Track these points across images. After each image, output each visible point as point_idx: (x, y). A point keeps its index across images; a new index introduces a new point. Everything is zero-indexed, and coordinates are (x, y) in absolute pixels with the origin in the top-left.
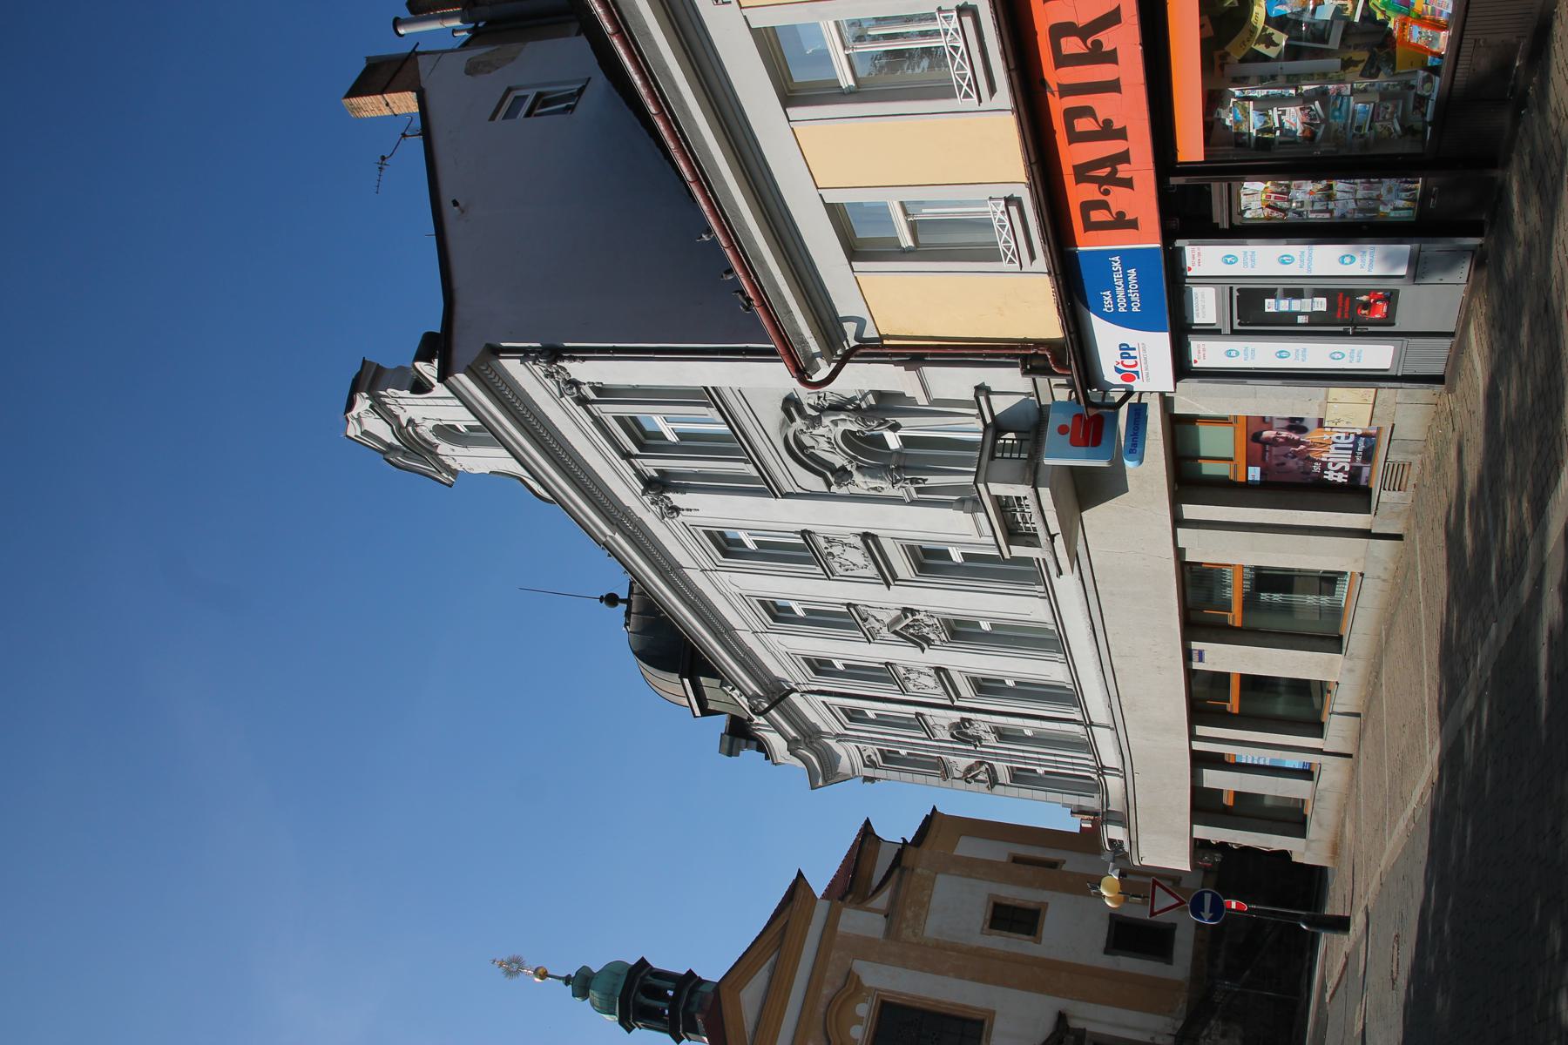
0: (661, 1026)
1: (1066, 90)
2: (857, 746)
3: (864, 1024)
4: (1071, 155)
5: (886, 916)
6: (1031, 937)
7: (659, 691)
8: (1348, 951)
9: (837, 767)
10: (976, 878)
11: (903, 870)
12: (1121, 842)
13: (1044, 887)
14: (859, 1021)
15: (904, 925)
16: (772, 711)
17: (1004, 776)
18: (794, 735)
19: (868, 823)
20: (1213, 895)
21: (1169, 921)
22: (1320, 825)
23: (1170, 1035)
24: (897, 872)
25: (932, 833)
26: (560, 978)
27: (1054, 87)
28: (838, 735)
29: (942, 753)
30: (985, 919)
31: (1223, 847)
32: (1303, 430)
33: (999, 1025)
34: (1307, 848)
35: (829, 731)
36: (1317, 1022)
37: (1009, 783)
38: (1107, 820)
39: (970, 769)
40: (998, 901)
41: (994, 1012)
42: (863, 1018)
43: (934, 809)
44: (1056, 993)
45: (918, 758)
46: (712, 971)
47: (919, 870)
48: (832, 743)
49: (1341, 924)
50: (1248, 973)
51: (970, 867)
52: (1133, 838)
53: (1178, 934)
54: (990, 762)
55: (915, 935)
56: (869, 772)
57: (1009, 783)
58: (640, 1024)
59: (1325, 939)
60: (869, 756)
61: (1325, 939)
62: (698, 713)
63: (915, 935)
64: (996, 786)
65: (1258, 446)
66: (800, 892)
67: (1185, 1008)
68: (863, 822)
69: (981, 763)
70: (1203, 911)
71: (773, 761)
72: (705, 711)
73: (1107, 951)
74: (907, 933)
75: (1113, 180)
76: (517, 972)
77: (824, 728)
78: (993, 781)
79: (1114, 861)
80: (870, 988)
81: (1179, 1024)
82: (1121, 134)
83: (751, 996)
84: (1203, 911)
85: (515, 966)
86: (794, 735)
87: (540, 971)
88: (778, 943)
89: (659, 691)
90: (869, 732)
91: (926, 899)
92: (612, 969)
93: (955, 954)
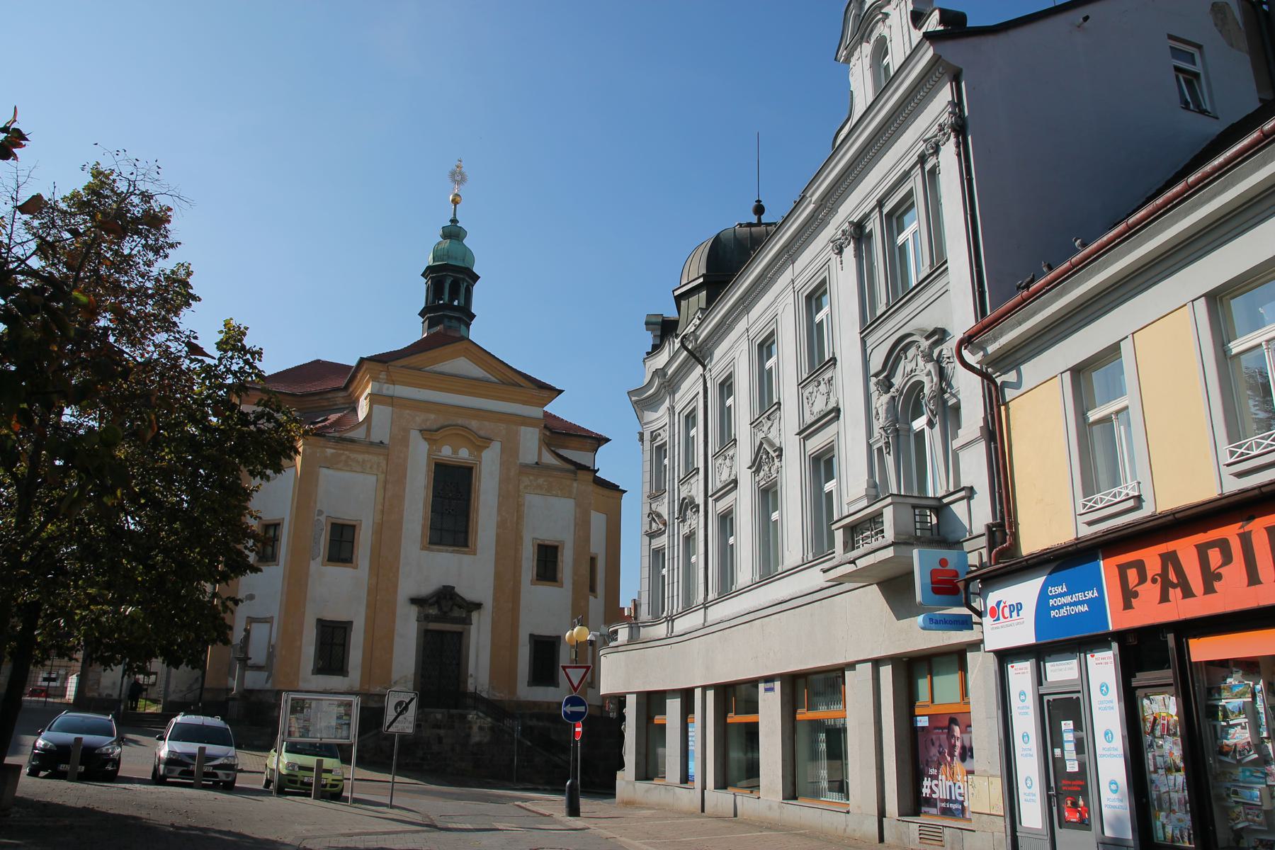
1: (1246, 539)
2: (666, 424)
3: (453, 456)
4: (1185, 548)
5: (537, 463)
7: (693, 253)
9: (648, 410)
11: (575, 473)
12: (616, 640)
14: (455, 452)
15: (531, 478)
16: (686, 352)
17: (657, 543)
18: (669, 373)
19: (607, 440)
22: (647, 791)
24: (571, 467)
25: (607, 492)
26: (455, 214)
27: (1247, 528)
29: (669, 492)
31: (622, 718)
32: (963, 759)
33: (466, 559)
34: (628, 782)
37: (652, 548)
39: (659, 516)
40: (559, 549)
41: (475, 554)
43: (625, 492)
45: (663, 474)
46: (477, 333)
47: (575, 485)
48: (667, 404)
50: (529, 743)
51: (583, 525)
52: (620, 649)
53: (551, 689)
55: (526, 487)
57: (652, 548)
58: (429, 282)
59: (561, 800)
60: (660, 435)
61: (561, 800)
62: (677, 293)
63: (526, 487)
64: (648, 538)
65: (946, 723)
66: (546, 394)
67: (496, 698)
69: (665, 524)
70: (571, 706)
72: (678, 299)
73: (531, 636)
74: (526, 480)
75: (1166, 586)
76: (455, 181)
77: (677, 396)
78: (652, 535)
81: (484, 695)
82: (1209, 589)
83: (462, 365)
85: (458, 178)
86: (669, 373)
87: (458, 199)
89: (693, 253)
90: (679, 432)
92: (467, 254)
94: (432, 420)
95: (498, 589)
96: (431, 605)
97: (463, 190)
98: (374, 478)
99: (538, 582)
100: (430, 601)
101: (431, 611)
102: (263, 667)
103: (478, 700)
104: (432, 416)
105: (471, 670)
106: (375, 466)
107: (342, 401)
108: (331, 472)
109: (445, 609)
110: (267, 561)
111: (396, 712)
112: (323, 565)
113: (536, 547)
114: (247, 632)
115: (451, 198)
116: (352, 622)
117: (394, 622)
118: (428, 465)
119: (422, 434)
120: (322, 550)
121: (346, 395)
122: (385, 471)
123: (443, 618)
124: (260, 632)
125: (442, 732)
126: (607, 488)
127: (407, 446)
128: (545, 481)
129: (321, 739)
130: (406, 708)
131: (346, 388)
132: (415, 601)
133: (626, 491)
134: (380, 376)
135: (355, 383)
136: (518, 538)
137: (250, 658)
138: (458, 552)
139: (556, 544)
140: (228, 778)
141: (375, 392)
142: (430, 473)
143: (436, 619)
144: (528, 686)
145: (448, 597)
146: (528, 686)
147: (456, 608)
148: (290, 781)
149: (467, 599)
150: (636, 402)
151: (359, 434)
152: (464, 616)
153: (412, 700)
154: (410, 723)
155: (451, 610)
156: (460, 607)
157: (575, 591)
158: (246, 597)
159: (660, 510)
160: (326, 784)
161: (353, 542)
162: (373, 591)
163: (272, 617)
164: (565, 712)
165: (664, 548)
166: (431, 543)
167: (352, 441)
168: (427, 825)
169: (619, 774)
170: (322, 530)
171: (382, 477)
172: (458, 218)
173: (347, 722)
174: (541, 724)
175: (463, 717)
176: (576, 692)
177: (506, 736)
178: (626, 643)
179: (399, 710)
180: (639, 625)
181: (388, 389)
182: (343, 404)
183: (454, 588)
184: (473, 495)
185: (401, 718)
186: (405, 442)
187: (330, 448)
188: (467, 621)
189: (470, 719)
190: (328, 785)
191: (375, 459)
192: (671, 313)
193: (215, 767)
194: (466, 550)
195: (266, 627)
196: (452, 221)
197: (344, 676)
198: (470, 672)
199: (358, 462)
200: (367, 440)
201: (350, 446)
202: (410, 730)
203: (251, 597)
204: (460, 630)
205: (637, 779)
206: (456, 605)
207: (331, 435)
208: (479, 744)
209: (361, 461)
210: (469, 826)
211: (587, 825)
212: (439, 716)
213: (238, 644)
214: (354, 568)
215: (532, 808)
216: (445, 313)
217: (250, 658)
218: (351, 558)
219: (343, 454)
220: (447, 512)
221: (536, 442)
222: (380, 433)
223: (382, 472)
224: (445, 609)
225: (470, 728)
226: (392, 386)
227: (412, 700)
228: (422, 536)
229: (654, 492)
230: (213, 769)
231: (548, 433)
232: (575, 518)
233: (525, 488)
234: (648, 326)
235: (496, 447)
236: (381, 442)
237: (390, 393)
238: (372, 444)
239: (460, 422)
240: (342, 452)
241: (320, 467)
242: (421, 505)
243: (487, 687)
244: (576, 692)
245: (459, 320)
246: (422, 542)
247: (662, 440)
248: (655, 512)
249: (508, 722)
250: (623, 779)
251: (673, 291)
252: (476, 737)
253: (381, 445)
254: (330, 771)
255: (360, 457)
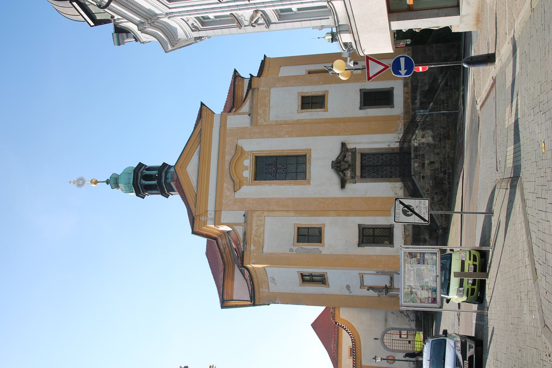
0: (156, 192)
2: (182, 19)
3: (249, 169)
5: (249, 115)
6: (322, 109)
7: (60, 12)
8: (494, 76)
9: (177, 36)
10: (290, 86)
11: (254, 89)
12: (351, 43)
13: (325, 83)
14: (246, 168)
15: (259, 118)
16: (112, 4)
17: (273, 18)
18: (139, 19)
19: (235, 71)
20: (406, 58)
21: (390, 87)
22: (468, 4)
23: (397, 142)
24: (250, 92)
25: (266, 68)
26: (104, 182)
28: (167, 14)
29: (231, 10)
30: (298, 105)
31: (411, 32)
33: (314, 155)
34: (461, 22)
35: (162, 13)
36: (472, 121)
37: (278, 21)
38: (340, 31)
39: (252, 18)
40: (303, 95)
41: (310, 150)
42: (248, 166)
43: (265, 56)
44: (339, 134)
45: (222, 19)
46: (172, 162)
47: (261, 89)
48: (166, 20)
49: (489, 59)
50: (432, 104)
51: (287, 81)
52: (357, 39)
53: (395, 92)
54: (262, 9)
55: (265, 121)
56: (197, 34)
57: (278, 21)
58: (147, 193)
59: (474, 72)
60: (193, 24)
61: (474, 72)
62: (92, 24)
63: (265, 121)
64: (271, 25)
66: (204, 113)
67: (403, 127)
68: (233, 72)
69: (256, 11)
70: (401, 70)
71: (140, 42)
72: (97, 22)
73: (361, 108)
74: (261, 121)
76: (83, 183)
77: (158, 12)
78: (268, 23)
79: (350, 57)
80: (248, 151)
81: (401, 136)
83: (192, 169)
84: (401, 70)
85: (81, 182)
86: (139, 19)
87: (94, 181)
88: (199, 141)
89: (60, 12)
90: (184, 7)
91: (267, 102)
92: (125, 172)
93: (286, 126)
94: (227, 185)
95: (332, 133)
96: (345, 175)
97: (88, 179)
98: (267, 218)
99: (326, 107)
100: (342, 176)
101: (349, 175)
102: (391, 277)
103: (405, 140)
104: (225, 185)
105: (385, 146)
106: (259, 218)
107: (225, 240)
108: (265, 246)
109: (347, 166)
110: (325, 279)
111: (412, 215)
112: (324, 246)
113: (303, 110)
114: (370, 288)
115: (94, 185)
116: (359, 225)
117: (357, 198)
118: (256, 185)
119: (237, 190)
120: (315, 247)
121: (220, 238)
122: (262, 212)
123: (352, 166)
124: (370, 281)
125: (427, 162)
126: (263, 68)
127: (245, 199)
128: (260, 109)
129: (437, 276)
130: (408, 207)
131: (215, 239)
132: (343, 186)
133: (265, 55)
134: (203, 220)
135: (211, 234)
136: (298, 122)
137: (386, 285)
138: (310, 160)
139: (300, 97)
140: (473, 347)
141: (213, 222)
142: (261, 183)
143: (354, 171)
144: (394, 108)
145: (339, 165)
146: (394, 108)
147: (346, 159)
148: (472, 294)
149: (339, 154)
150: (173, 46)
151: (240, 231)
152: (350, 153)
153: (401, 203)
154: (420, 203)
155: (347, 162)
156: (345, 156)
157: (330, 83)
158: (348, 290)
159: (248, 18)
160: (473, 265)
161: (308, 228)
162: (339, 213)
163: (359, 274)
164: (406, 74)
165: (276, 10)
166: (305, 178)
167: (245, 234)
168: (513, 187)
169: (454, 30)
170: (302, 248)
171: (266, 213)
172: (105, 180)
173: (422, 255)
174: (418, 97)
175: (416, 149)
176: (389, 67)
177: (427, 119)
178: (352, 34)
179: (410, 213)
180: (337, 25)
181: (211, 214)
182: (226, 239)
183: (333, 162)
184: (273, 154)
185: (417, 211)
186: (242, 201)
187: (250, 248)
188: (354, 151)
189: (417, 145)
190: (474, 263)
191: (255, 219)
192: (110, 27)
193: (464, 358)
194: (308, 156)
195: (365, 276)
196: (108, 183)
197: (394, 227)
198: (387, 147)
199: (257, 229)
200: (243, 225)
201: (248, 235)
202: (425, 203)
203: (348, 287)
204: (360, 155)
205: (458, 13)
206: (344, 159)
207: (242, 248)
208: (433, 137)
209: (257, 227)
210: (511, 149)
211: (509, 38)
212: (416, 165)
213: (378, 293)
214: (325, 226)
215: (484, 94)
216: (163, 182)
217: (386, 285)
218: (319, 228)
219: (253, 239)
220: (285, 170)
221: (236, 116)
222: (238, 216)
223: (263, 213)
224: (347, 166)
225: (423, 144)
226: (209, 212)
227: (401, 203)
228: (302, 184)
229: (236, 24)
230: (466, 360)
231: (234, 110)
232: (282, 86)
233: (266, 122)
234: (121, 43)
235: (241, 143)
236: (244, 215)
237: (213, 213)
238: (245, 222)
239: (227, 167)
240: (252, 240)
241: (263, 252)
242: (282, 187)
243: (396, 134)
244: (389, 67)
245: (166, 173)
246: (305, 184)
247: (196, 22)
248: (250, 22)
249: (418, 119)
250: (459, 26)
251: (91, 26)
252: (429, 139)
253: (246, 215)
254: (463, 263)
255: (255, 228)
